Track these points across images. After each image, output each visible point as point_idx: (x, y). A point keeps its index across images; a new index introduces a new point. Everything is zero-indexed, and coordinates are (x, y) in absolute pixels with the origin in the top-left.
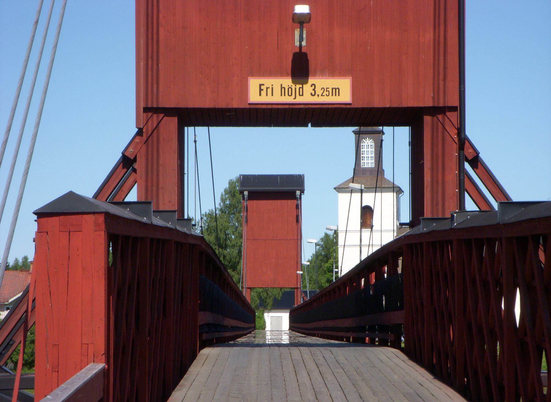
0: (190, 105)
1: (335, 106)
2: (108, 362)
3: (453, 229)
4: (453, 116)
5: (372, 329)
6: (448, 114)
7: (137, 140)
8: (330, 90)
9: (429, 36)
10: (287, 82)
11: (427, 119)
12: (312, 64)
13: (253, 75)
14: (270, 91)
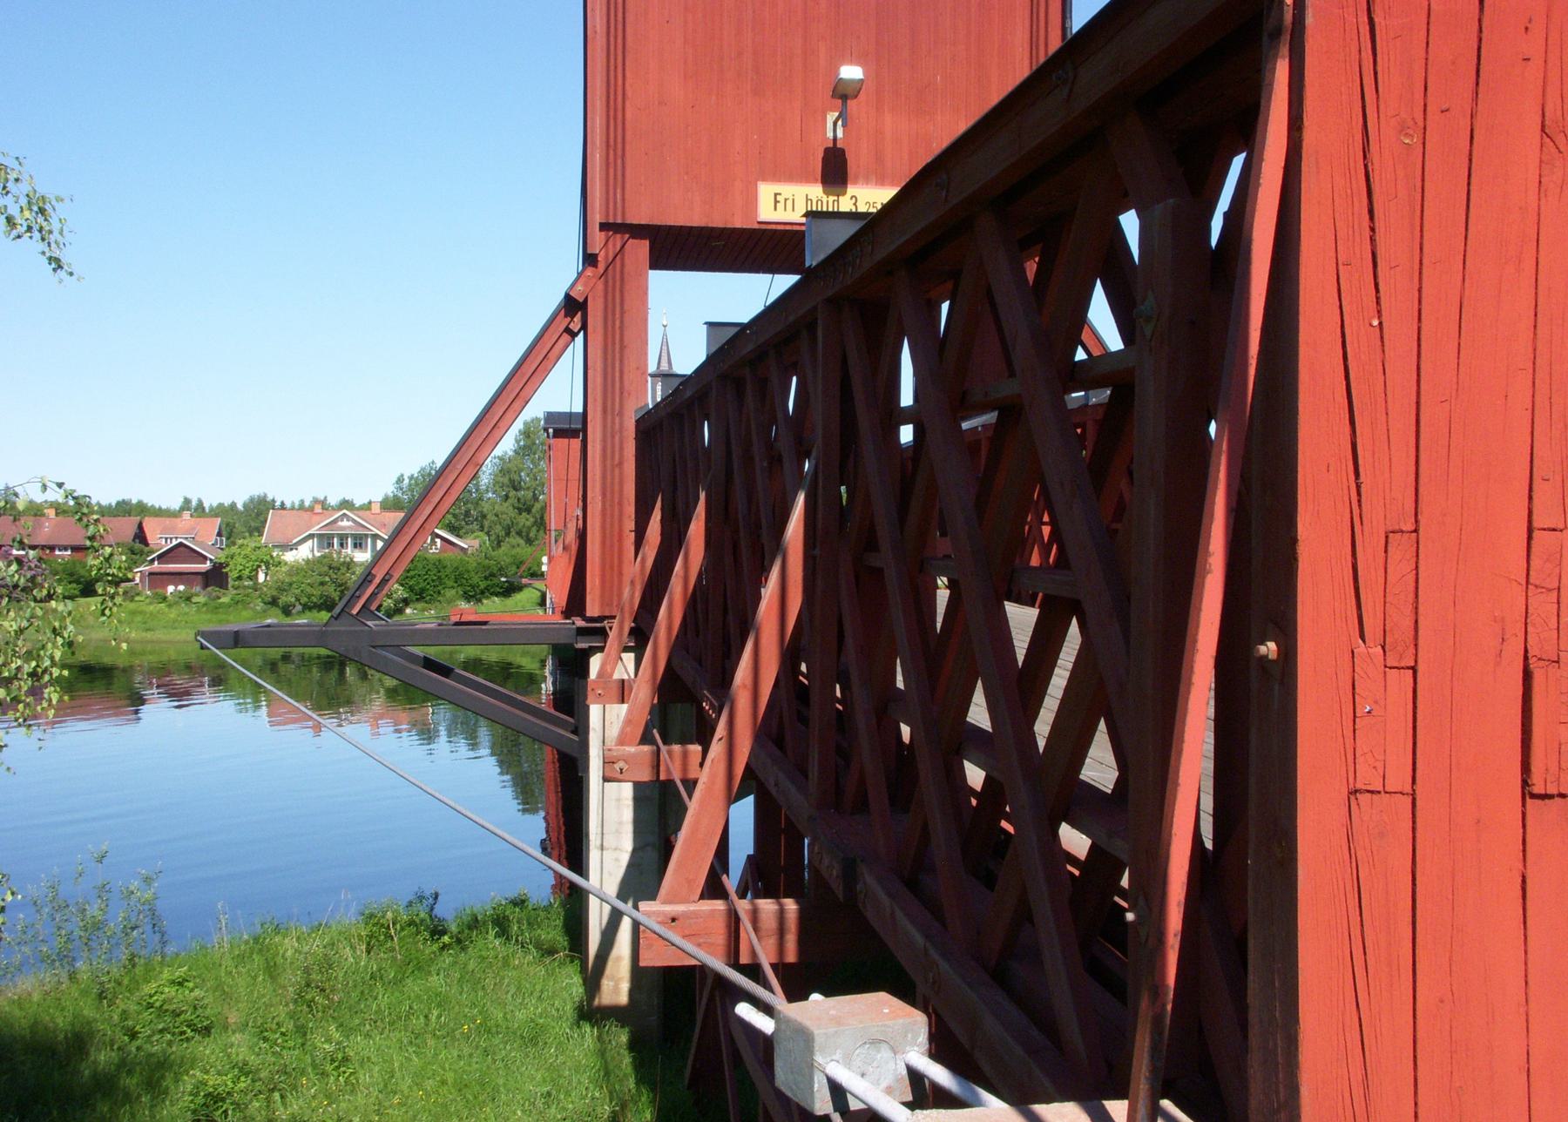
14: (789, 203)
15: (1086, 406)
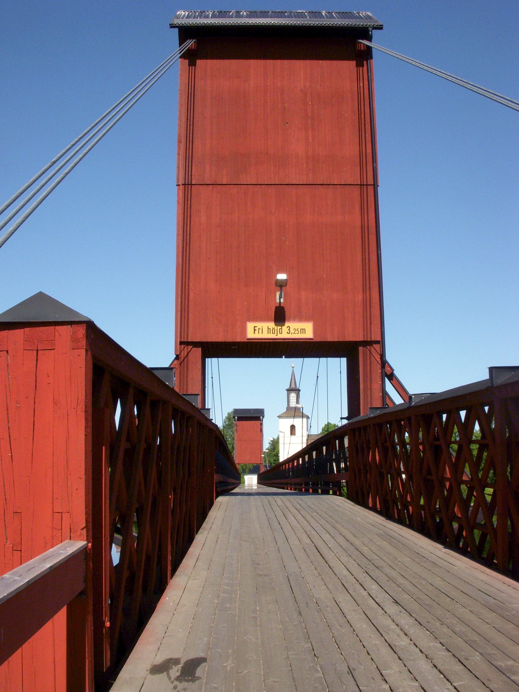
0: (209, 340)
1: (303, 340)
2: (88, 540)
3: (412, 407)
4: (377, 347)
5: (291, 484)
6: (374, 345)
7: (175, 363)
8: (299, 330)
9: (360, 297)
10: (272, 325)
11: (361, 348)
12: (287, 314)
13: (250, 320)
14: (260, 330)
15: (492, 386)
